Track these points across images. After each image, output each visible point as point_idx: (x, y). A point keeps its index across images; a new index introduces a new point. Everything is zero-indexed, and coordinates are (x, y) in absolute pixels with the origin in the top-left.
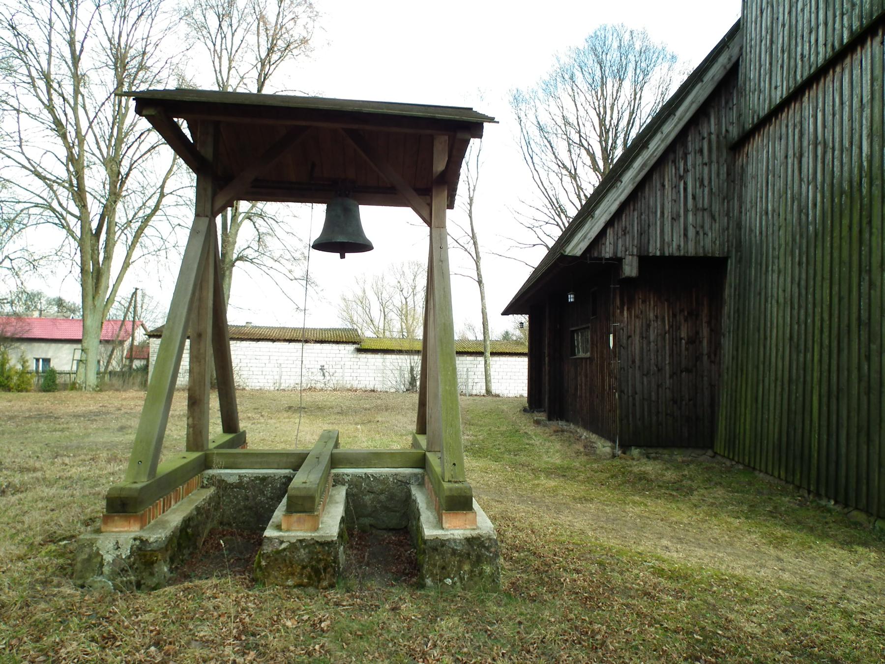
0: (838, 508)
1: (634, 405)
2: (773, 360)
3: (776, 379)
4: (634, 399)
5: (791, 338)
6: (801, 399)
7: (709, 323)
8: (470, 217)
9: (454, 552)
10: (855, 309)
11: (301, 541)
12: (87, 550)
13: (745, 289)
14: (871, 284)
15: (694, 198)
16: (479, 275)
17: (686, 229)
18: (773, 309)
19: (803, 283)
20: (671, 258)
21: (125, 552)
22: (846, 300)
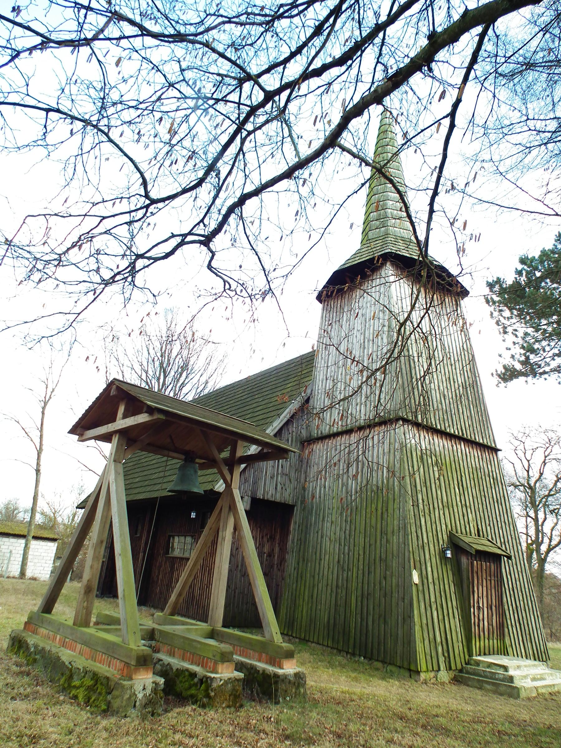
0: (366, 661)
1: (235, 596)
2: (326, 573)
3: (327, 585)
4: (235, 593)
5: (338, 562)
6: (344, 598)
7: (279, 544)
8: (43, 413)
9: (290, 682)
10: (378, 552)
11: (229, 679)
12: (129, 691)
13: (307, 527)
14: (387, 541)
15: (282, 467)
16: (38, 464)
17: (276, 485)
18: (326, 543)
19: (347, 532)
20: (268, 501)
21: (148, 692)
22: (373, 547)
